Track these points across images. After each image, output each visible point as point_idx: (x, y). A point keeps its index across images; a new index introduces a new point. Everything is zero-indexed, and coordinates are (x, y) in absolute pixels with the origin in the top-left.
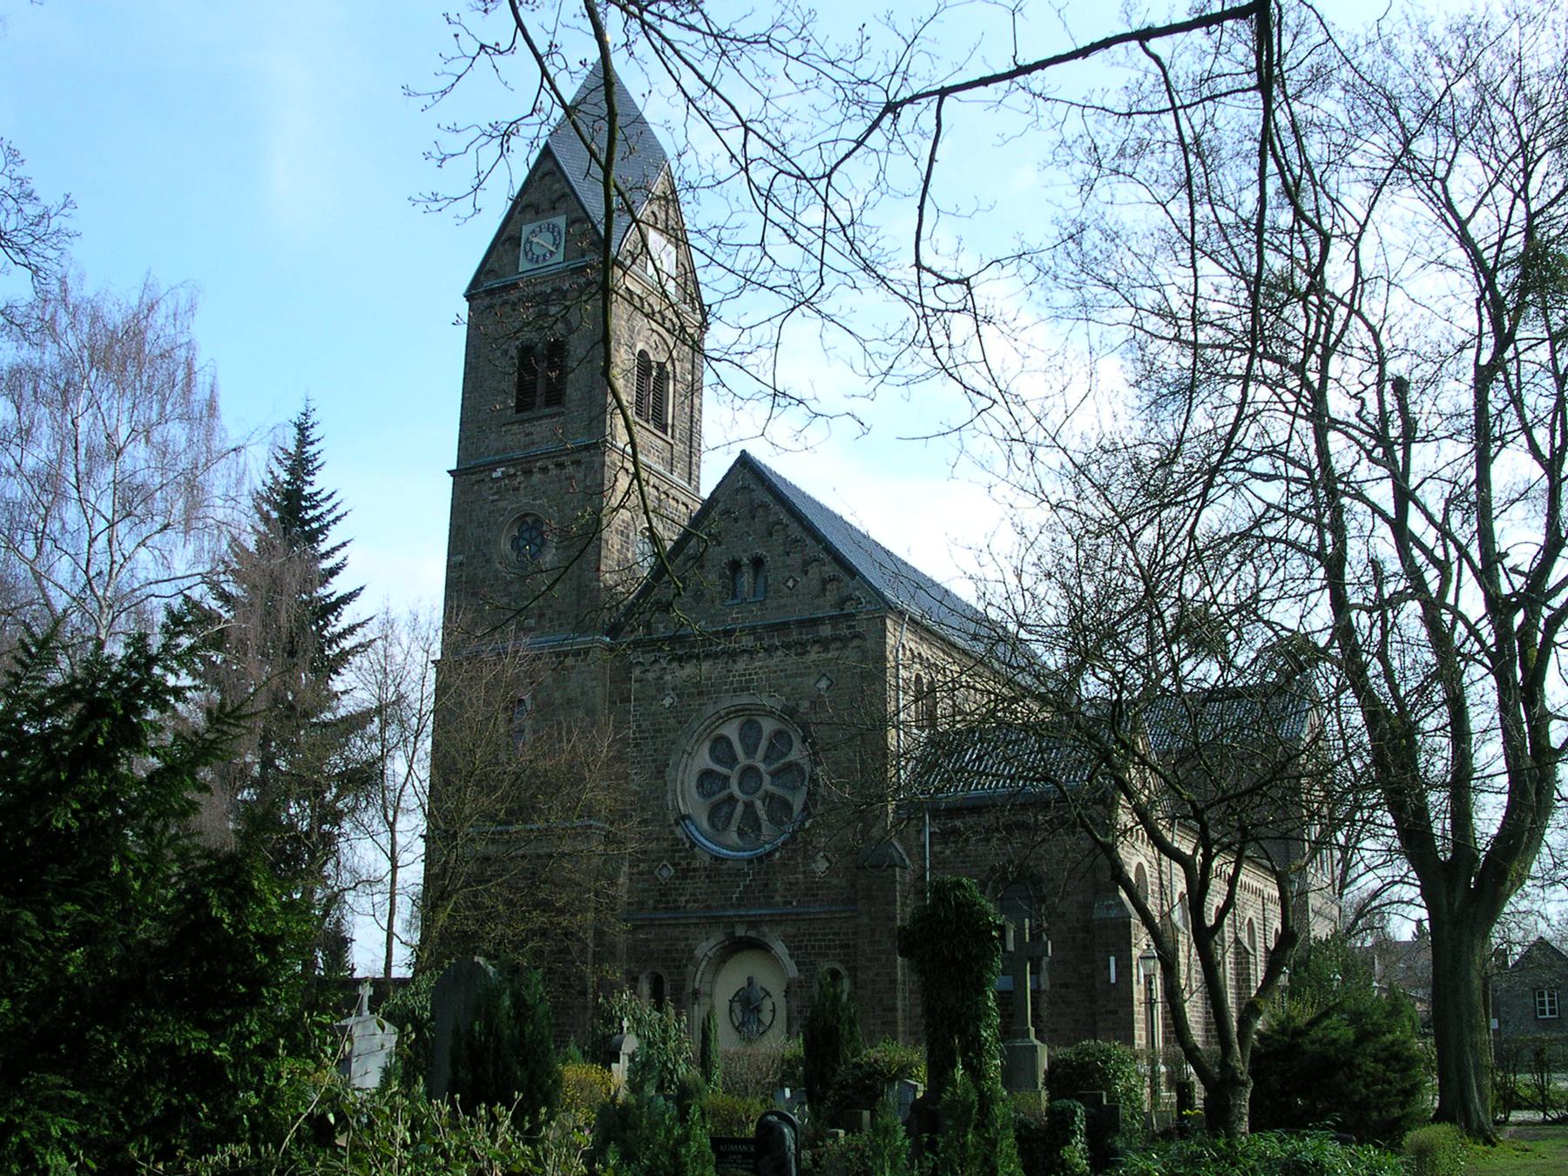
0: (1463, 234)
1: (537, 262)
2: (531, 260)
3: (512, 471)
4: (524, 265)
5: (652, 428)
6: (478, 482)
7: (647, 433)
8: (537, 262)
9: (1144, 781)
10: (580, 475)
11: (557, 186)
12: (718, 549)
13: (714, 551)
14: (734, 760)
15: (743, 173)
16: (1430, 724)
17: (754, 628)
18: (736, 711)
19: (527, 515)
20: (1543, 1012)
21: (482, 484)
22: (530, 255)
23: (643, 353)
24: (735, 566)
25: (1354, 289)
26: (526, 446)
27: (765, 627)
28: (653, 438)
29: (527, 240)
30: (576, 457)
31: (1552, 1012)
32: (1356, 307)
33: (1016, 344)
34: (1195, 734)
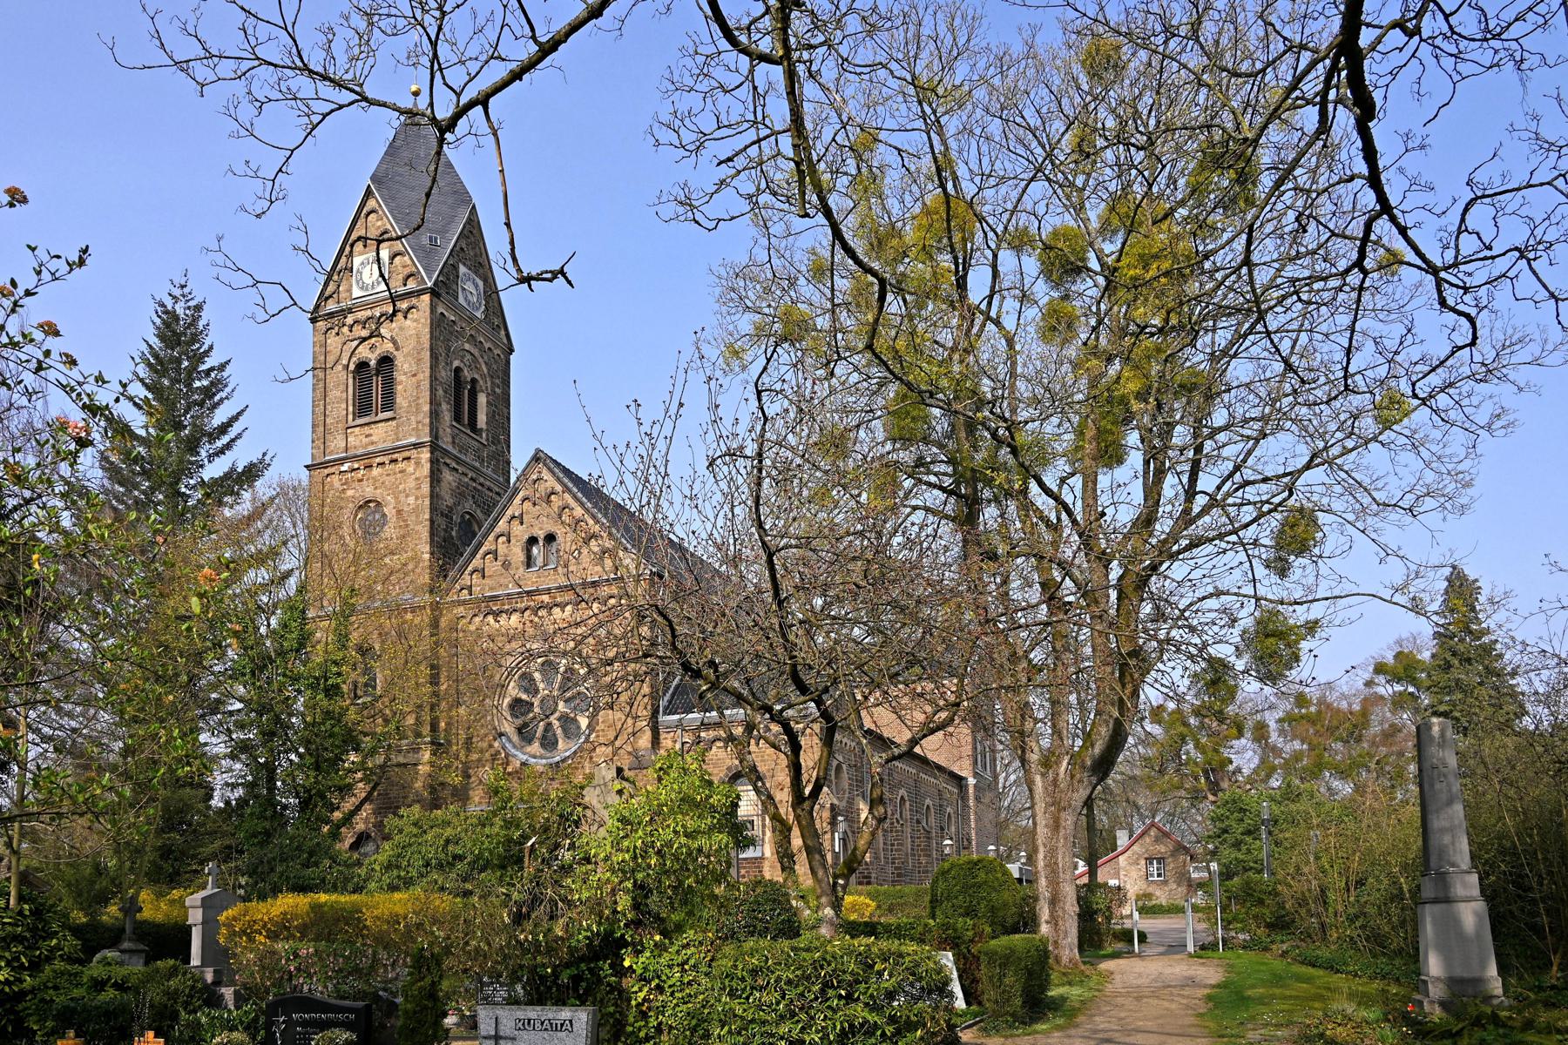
0: (1429, 266)
2: (362, 288)
3: (356, 466)
4: (357, 292)
5: (468, 432)
9: (18, 713)
11: (379, 223)
13: (517, 529)
15: (1255, 258)
17: (549, 589)
19: (370, 501)
20: (1152, 875)
23: (458, 370)
24: (533, 541)
25: (991, 297)
26: (367, 445)
27: (557, 588)
28: (470, 441)
29: (358, 271)
30: (406, 454)
31: (1159, 875)
32: (993, 314)
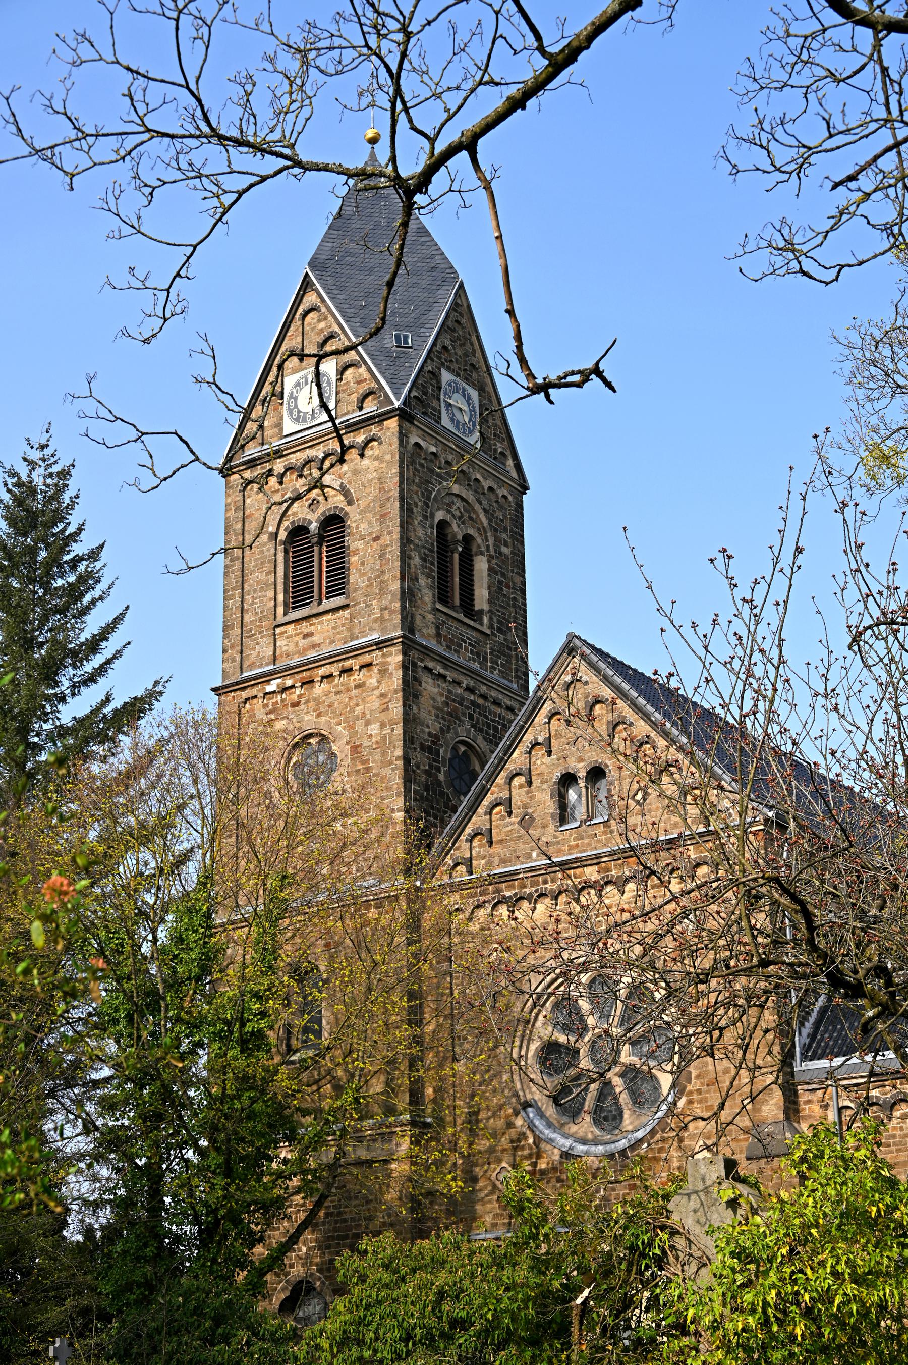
1: (304, 421)
2: (297, 420)
3: (289, 683)
4: (289, 426)
6: (247, 700)
7: (455, 624)
8: (304, 421)
10: (373, 682)
11: (322, 325)
12: (546, 760)
14: (583, 1029)
16: (145, 855)
18: (523, 727)
19: (311, 736)
21: (255, 701)
22: (295, 413)
23: (443, 525)
24: (568, 779)
26: (305, 650)
28: (463, 629)
33: (703, 685)
34: (659, 878)
